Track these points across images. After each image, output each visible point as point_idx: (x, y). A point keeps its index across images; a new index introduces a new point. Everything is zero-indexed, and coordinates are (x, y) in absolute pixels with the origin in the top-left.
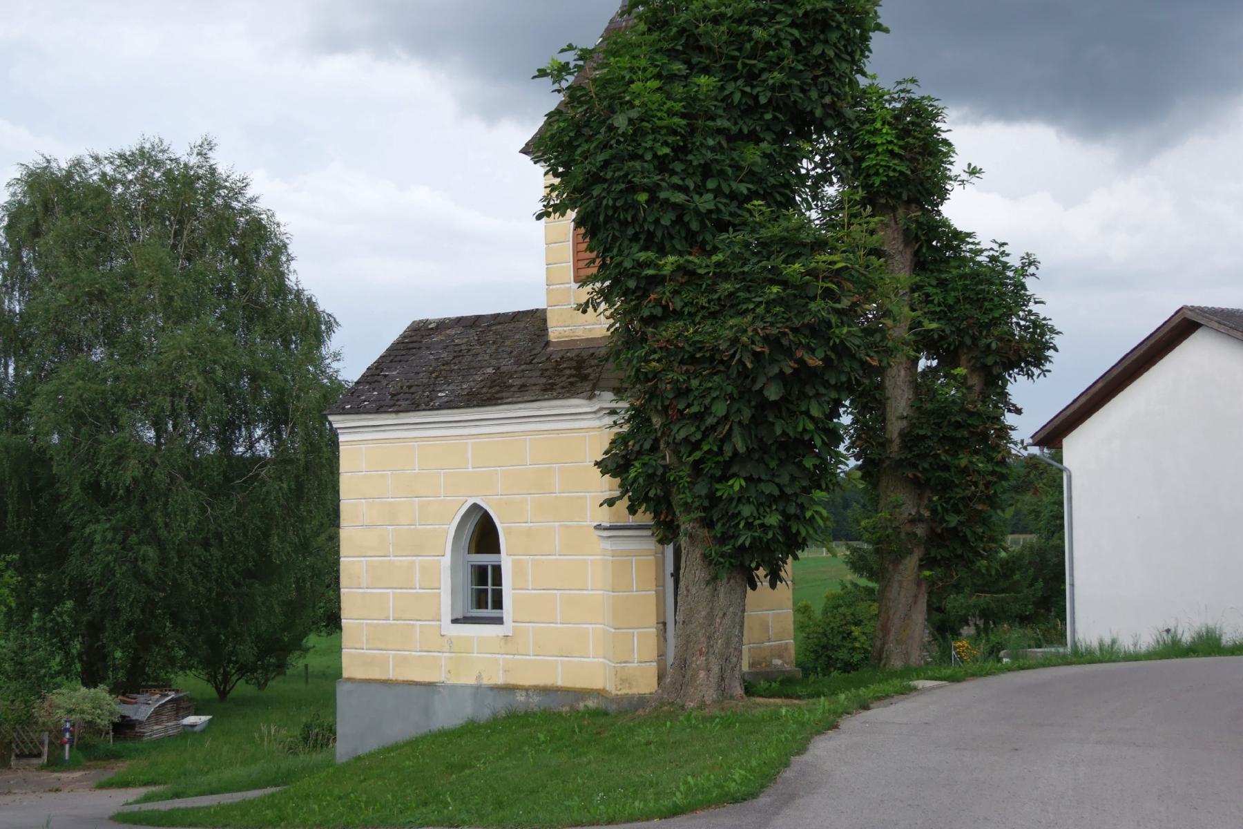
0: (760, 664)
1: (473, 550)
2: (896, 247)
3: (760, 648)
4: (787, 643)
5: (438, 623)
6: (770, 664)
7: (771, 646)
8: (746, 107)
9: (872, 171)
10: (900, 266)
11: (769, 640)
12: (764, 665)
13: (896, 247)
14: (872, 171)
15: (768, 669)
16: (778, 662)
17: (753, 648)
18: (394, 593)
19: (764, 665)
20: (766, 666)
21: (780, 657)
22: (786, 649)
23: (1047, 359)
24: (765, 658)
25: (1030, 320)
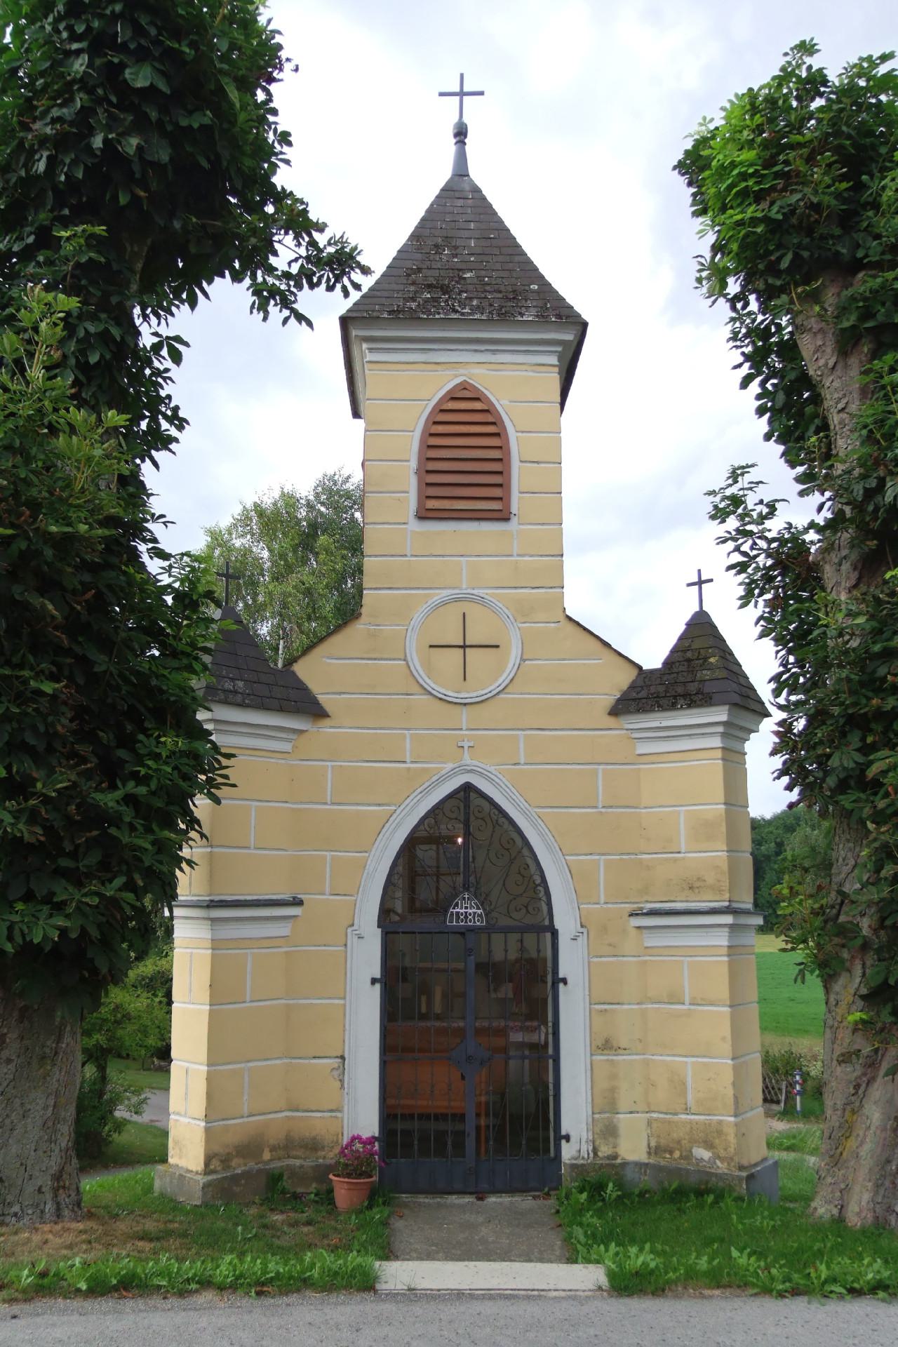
0: (671, 1153)
1: (156, 1078)
2: (822, 362)
3: (669, 1122)
4: (720, 1122)
5: (342, 1002)
6: (688, 1156)
7: (691, 1122)
8: (752, 298)
9: (105, 438)
10: (836, 396)
11: (687, 1111)
12: (677, 1154)
13: (822, 362)
14: (105, 438)
15: (683, 1164)
16: (703, 1154)
17: (656, 1120)
18: (604, 770)
19: (677, 1154)
20: (681, 1157)
21: (709, 1145)
22: (720, 1133)
23: (279, 47)
24: (679, 1142)
25: (178, 137)
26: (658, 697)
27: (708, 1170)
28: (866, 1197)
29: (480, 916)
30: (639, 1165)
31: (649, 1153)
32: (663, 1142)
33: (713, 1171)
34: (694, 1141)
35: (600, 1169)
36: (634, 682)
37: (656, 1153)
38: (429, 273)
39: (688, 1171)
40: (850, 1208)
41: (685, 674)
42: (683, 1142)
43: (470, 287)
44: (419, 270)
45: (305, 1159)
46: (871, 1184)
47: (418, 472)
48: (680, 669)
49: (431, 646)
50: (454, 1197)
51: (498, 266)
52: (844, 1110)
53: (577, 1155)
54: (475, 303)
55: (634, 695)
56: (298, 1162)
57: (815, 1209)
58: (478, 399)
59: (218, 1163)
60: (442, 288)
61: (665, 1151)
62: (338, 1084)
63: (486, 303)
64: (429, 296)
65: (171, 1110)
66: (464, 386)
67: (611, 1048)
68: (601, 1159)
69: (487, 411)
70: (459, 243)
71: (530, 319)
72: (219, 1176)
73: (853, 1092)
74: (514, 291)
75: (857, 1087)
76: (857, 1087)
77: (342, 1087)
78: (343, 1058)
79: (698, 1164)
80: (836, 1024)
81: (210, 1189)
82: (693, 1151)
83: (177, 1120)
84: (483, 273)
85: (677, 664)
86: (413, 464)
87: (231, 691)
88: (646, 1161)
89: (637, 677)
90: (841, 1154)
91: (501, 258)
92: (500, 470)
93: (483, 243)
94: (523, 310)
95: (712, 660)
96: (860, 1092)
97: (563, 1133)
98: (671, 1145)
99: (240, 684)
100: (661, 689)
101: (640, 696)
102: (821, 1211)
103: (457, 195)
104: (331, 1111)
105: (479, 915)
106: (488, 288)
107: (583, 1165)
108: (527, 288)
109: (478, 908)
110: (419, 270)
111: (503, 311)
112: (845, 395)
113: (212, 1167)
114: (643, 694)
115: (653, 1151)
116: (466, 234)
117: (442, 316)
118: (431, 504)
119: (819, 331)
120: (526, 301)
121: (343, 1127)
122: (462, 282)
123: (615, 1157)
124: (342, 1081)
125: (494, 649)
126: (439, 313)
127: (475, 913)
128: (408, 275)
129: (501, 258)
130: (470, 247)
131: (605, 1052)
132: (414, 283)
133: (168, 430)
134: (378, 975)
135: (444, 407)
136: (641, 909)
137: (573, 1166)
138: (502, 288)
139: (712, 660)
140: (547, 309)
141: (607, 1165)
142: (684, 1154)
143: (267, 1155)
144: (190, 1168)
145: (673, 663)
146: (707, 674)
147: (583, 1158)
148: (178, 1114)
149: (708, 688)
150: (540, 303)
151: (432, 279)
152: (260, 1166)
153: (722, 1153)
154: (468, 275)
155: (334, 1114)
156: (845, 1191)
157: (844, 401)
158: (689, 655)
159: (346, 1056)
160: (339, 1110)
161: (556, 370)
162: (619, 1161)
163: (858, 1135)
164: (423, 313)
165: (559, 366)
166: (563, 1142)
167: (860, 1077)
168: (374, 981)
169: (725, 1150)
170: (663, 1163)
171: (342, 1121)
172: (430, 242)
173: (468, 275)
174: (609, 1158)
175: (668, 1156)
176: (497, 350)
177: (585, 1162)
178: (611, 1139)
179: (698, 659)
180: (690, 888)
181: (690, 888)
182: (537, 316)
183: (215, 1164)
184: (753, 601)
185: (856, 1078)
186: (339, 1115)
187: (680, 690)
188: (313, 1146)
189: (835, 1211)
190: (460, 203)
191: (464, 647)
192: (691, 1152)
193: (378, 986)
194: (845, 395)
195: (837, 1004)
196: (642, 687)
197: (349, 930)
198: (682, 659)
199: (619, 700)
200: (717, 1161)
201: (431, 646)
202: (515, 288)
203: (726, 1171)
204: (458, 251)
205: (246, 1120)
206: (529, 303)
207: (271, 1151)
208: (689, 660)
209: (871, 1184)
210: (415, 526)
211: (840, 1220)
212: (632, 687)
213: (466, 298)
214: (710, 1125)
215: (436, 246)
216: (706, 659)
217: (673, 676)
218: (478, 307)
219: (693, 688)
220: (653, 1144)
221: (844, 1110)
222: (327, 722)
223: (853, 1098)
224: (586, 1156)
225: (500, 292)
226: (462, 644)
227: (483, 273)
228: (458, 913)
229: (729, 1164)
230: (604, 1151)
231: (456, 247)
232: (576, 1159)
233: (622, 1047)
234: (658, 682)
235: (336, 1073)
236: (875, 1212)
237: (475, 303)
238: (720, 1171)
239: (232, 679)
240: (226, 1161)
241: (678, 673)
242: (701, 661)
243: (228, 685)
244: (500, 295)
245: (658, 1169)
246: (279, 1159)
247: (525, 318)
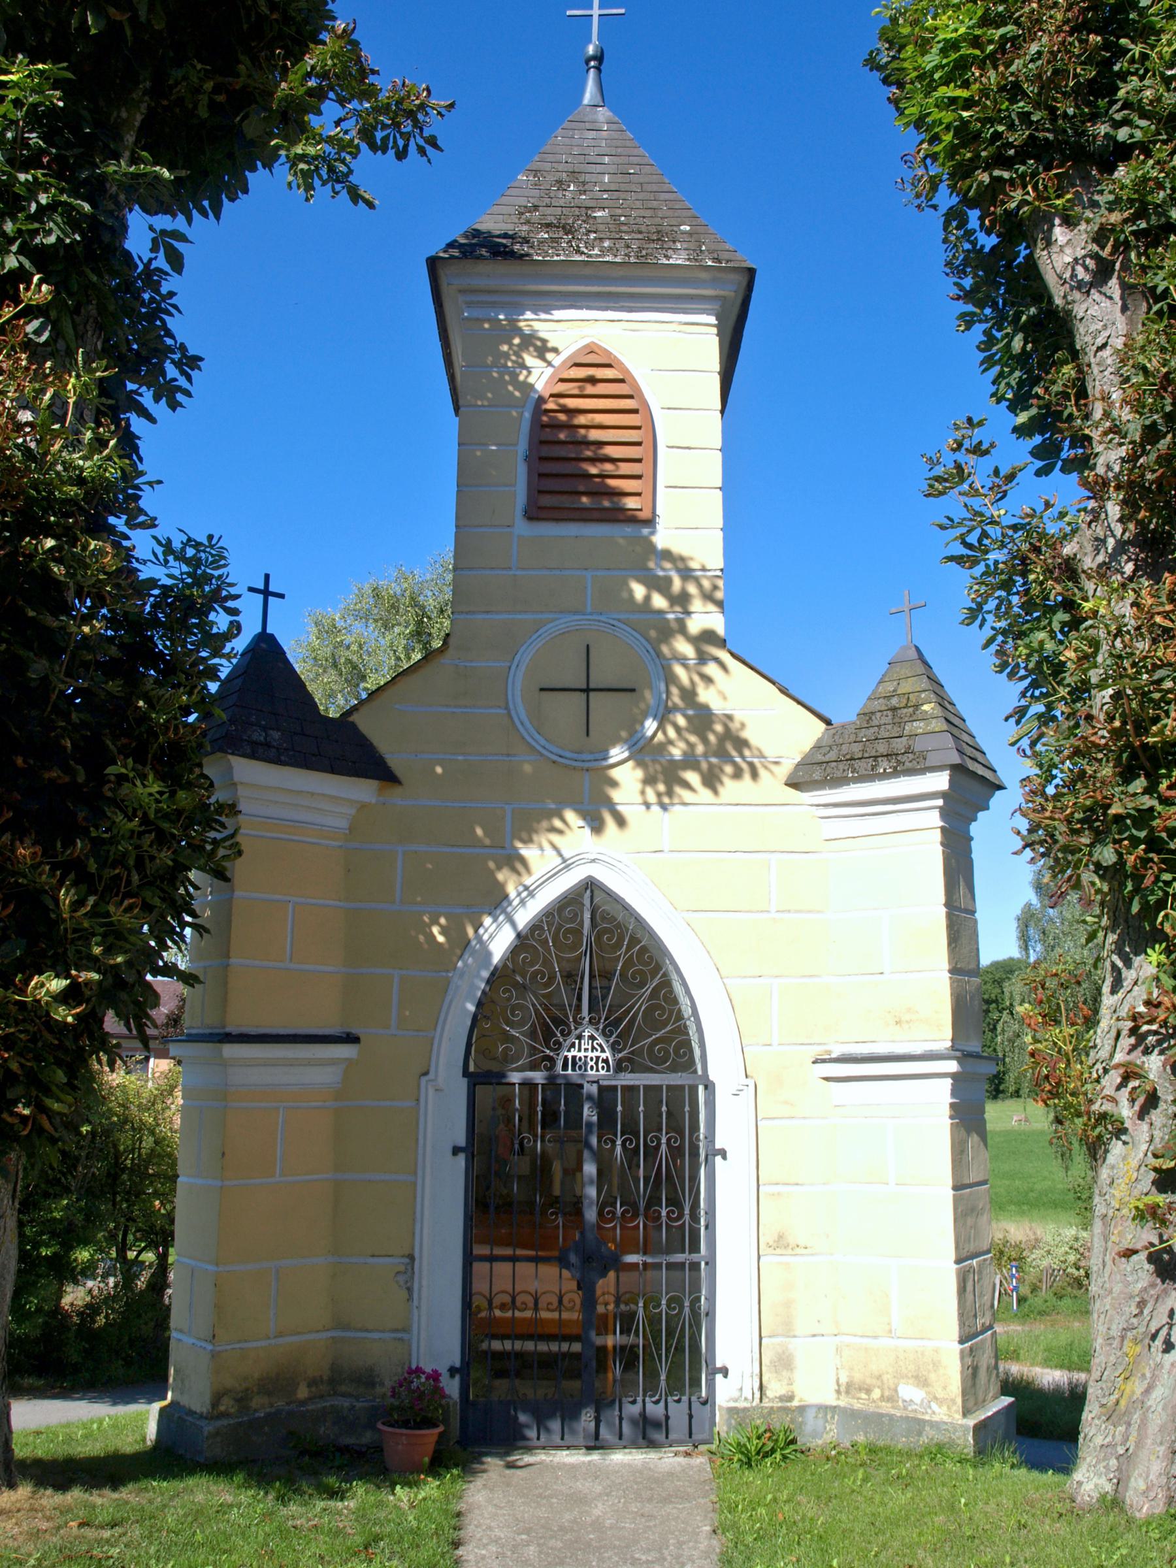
0: (868, 1391)
12: (876, 1394)
15: (886, 1408)
16: (910, 1393)
19: (876, 1394)
20: (882, 1398)
21: (921, 1381)
22: (936, 1365)
24: (879, 1377)
26: (852, 759)
27: (920, 1417)
28: (1157, 1467)
29: (606, 1061)
30: (824, 1409)
31: (838, 1392)
32: (858, 1377)
33: (927, 1417)
34: (900, 1376)
35: (770, 1414)
36: (819, 740)
37: (847, 1392)
38: (549, 211)
39: (891, 1417)
40: (1132, 1483)
41: (889, 727)
42: (885, 1377)
43: (601, 227)
44: (536, 207)
45: (357, 1398)
46: (1163, 1448)
47: (527, 459)
48: (882, 722)
49: (542, 690)
50: (565, 1453)
51: (638, 204)
52: (1123, 1338)
53: (736, 1394)
54: (606, 244)
55: (820, 758)
56: (346, 1403)
57: (1080, 1483)
58: (609, 366)
59: (232, 1402)
60: (564, 228)
61: (860, 1389)
62: (404, 1294)
63: (621, 244)
64: (546, 236)
65: (172, 1325)
66: (591, 349)
67: (786, 1246)
68: (771, 1400)
69: (622, 381)
70: (588, 178)
71: (679, 262)
72: (232, 1422)
73: (1136, 1312)
74: (658, 232)
75: (1142, 1304)
76: (1142, 1304)
77: (410, 1298)
78: (412, 1258)
79: (905, 1408)
80: (1110, 1213)
81: (219, 1439)
82: (899, 1389)
83: (180, 1340)
84: (619, 212)
85: (879, 715)
86: (522, 447)
87: (261, 744)
88: (834, 1403)
89: (824, 734)
90: (1117, 1403)
91: (641, 196)
92: (639, 473)
93: (620, 178)
94: (670, 252)
95: (926, 707)
96: (1146, 1312)
97: (719, 1364)
98: (868, 1381)
99: (276, 735)
100: (856, 749)
101: (827, 759)
102: (1088, 1487)
103: (588, 126)
104: (396, 1330)
105: (604, 1061)
106: (624, 228)
107: (745, 1409)
108: (675, 229)
109: (603, 1051)
110: (536, 207)
111: (644, 253)
112: (1105, 327)
113: (222, 1408)
114: (832, 755)
115: (843, 1389)
116: (599, 168)
117: (562, 258)
118: (546, 500)
119: (1067, 243)
120: (674, 242)
121: (410, 1355)
122: (591, 221)
123: (791, 1398)
124: (410, 1290)
125: (629, 694)
126: (558, 255)
127: (598, 1058)
128: (521, 214)
129: (641, 196)
130: (602, 182)
131: (778, 1251)
132: (528, 222)
133: (176, 380)
134: (461, 1141)
135: (565, 376)
136: (829, 1052)
137: (732, 1411)
138: (643, 228)
139: (926, 707)
140: (701, 251)
141: (780, 1408)
142: (887, 1393)
143: (303, 1393)
144: (194, 1409)
145: (872, 713)
146: (919, 727)
147: (746, 1399)
148: (181, 1331)
149: (918, 746)
150: (692, 246)
151: (552, 218)
152: (293, 1406)
153: (940, 1394)
154: (599, 214)
155: (399, 1335)
156: (1127, 1459)
157: (1105, 334)
158: (894, 702)
159: (417, 1255)
160: (406, 1329)
161: (715, 330)
162: (795, 1403)
163: (1143, 1375)
164: (537, 254)
165: (720, 327)
166: (719, 1377)
167: (1145, 1289)
168: (456, 1151)
169: (945, 1388)
170: (857, 1405)
171: (410, 1346)
172: (551, 178)
173: (599, 214)
174: (781, 1399)
175: (864, 1396)
176: (632, 296)
177: (747, 1405)
178: (785, 1373)
179: (906, 707)
180: (897, 1023)
181: (897, 1023)
182: (689, 259)
183: (226, 1405)
184: (980, 617)
185: (1141, 1291)
186: (405, 1336)
187: (882, 748)
188: (367, 1379)
189: (1108, 1487)
190: (592, 134)
191: (587, 690)
192: (896, 1391)
193: (461, 1159)
194: (1105, 327)
195: (1112, 1182)
196: (830, 747)
197: (424, 1079)
198: (884, 708)
199: (798, 765)
200: (933, 1405)
201: (542, 690)
202: (660, 228)
203: (946, 1419)
204: (586, 187)
205: (273, 1342)
206: (679, 246)
207: (309, 1386)
208: (894, 709)
209: (1163, 1448)
210: (523, 528)
211: (1114, 1503)
212: (817, 747)
213: (595, 239)
214: (923, 1354)
215: (560, 182)
216: (917, 707)
217: (872, 730)
218: (610, 249)
219: (899, 745)
220: (844, 1380)
221: (1123, 1338)
222: (398, 790)
223: (1135, 1321)
224: (750, 1397)
225: (640, 232)
226: (584, 687)
227: (619, 212)
228: (574, 1057)
229: (949, 1408)
230: (775, 1389)
231: (584, 183)
232: (736, 1400)
233: (802, 1244)
234: (853, 738)
235: (401, 1279)
236: (1169, 1489)
237: (606, 244)
238: (936, 1418)
239: (265, 729)
240: (242, 1400)
241: (879, 726)
242: (911, 710)
243: (258, 736)
244: (640, 236)
245: (849, 1415)
246: (322, 1397)
247: (671, 261)
